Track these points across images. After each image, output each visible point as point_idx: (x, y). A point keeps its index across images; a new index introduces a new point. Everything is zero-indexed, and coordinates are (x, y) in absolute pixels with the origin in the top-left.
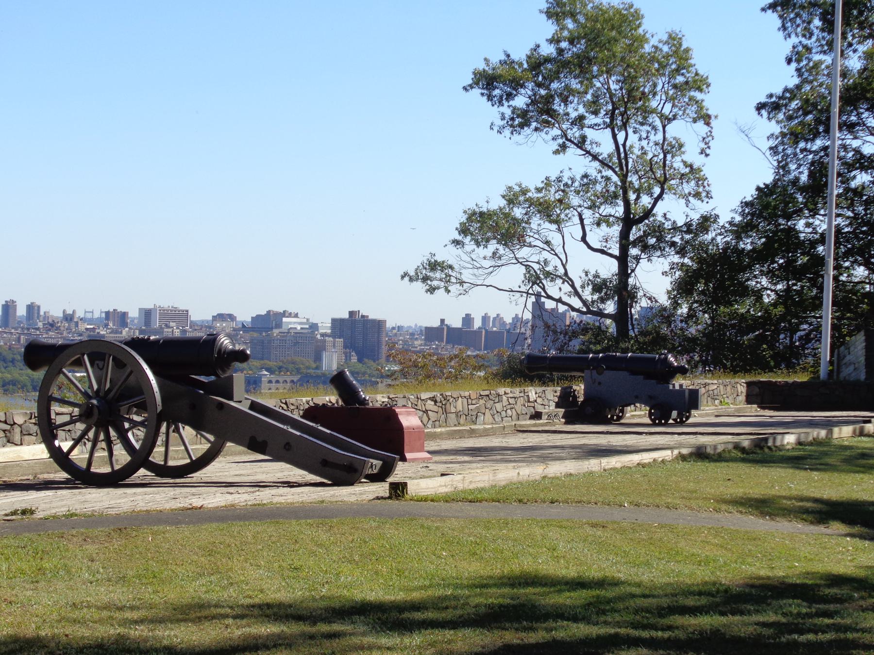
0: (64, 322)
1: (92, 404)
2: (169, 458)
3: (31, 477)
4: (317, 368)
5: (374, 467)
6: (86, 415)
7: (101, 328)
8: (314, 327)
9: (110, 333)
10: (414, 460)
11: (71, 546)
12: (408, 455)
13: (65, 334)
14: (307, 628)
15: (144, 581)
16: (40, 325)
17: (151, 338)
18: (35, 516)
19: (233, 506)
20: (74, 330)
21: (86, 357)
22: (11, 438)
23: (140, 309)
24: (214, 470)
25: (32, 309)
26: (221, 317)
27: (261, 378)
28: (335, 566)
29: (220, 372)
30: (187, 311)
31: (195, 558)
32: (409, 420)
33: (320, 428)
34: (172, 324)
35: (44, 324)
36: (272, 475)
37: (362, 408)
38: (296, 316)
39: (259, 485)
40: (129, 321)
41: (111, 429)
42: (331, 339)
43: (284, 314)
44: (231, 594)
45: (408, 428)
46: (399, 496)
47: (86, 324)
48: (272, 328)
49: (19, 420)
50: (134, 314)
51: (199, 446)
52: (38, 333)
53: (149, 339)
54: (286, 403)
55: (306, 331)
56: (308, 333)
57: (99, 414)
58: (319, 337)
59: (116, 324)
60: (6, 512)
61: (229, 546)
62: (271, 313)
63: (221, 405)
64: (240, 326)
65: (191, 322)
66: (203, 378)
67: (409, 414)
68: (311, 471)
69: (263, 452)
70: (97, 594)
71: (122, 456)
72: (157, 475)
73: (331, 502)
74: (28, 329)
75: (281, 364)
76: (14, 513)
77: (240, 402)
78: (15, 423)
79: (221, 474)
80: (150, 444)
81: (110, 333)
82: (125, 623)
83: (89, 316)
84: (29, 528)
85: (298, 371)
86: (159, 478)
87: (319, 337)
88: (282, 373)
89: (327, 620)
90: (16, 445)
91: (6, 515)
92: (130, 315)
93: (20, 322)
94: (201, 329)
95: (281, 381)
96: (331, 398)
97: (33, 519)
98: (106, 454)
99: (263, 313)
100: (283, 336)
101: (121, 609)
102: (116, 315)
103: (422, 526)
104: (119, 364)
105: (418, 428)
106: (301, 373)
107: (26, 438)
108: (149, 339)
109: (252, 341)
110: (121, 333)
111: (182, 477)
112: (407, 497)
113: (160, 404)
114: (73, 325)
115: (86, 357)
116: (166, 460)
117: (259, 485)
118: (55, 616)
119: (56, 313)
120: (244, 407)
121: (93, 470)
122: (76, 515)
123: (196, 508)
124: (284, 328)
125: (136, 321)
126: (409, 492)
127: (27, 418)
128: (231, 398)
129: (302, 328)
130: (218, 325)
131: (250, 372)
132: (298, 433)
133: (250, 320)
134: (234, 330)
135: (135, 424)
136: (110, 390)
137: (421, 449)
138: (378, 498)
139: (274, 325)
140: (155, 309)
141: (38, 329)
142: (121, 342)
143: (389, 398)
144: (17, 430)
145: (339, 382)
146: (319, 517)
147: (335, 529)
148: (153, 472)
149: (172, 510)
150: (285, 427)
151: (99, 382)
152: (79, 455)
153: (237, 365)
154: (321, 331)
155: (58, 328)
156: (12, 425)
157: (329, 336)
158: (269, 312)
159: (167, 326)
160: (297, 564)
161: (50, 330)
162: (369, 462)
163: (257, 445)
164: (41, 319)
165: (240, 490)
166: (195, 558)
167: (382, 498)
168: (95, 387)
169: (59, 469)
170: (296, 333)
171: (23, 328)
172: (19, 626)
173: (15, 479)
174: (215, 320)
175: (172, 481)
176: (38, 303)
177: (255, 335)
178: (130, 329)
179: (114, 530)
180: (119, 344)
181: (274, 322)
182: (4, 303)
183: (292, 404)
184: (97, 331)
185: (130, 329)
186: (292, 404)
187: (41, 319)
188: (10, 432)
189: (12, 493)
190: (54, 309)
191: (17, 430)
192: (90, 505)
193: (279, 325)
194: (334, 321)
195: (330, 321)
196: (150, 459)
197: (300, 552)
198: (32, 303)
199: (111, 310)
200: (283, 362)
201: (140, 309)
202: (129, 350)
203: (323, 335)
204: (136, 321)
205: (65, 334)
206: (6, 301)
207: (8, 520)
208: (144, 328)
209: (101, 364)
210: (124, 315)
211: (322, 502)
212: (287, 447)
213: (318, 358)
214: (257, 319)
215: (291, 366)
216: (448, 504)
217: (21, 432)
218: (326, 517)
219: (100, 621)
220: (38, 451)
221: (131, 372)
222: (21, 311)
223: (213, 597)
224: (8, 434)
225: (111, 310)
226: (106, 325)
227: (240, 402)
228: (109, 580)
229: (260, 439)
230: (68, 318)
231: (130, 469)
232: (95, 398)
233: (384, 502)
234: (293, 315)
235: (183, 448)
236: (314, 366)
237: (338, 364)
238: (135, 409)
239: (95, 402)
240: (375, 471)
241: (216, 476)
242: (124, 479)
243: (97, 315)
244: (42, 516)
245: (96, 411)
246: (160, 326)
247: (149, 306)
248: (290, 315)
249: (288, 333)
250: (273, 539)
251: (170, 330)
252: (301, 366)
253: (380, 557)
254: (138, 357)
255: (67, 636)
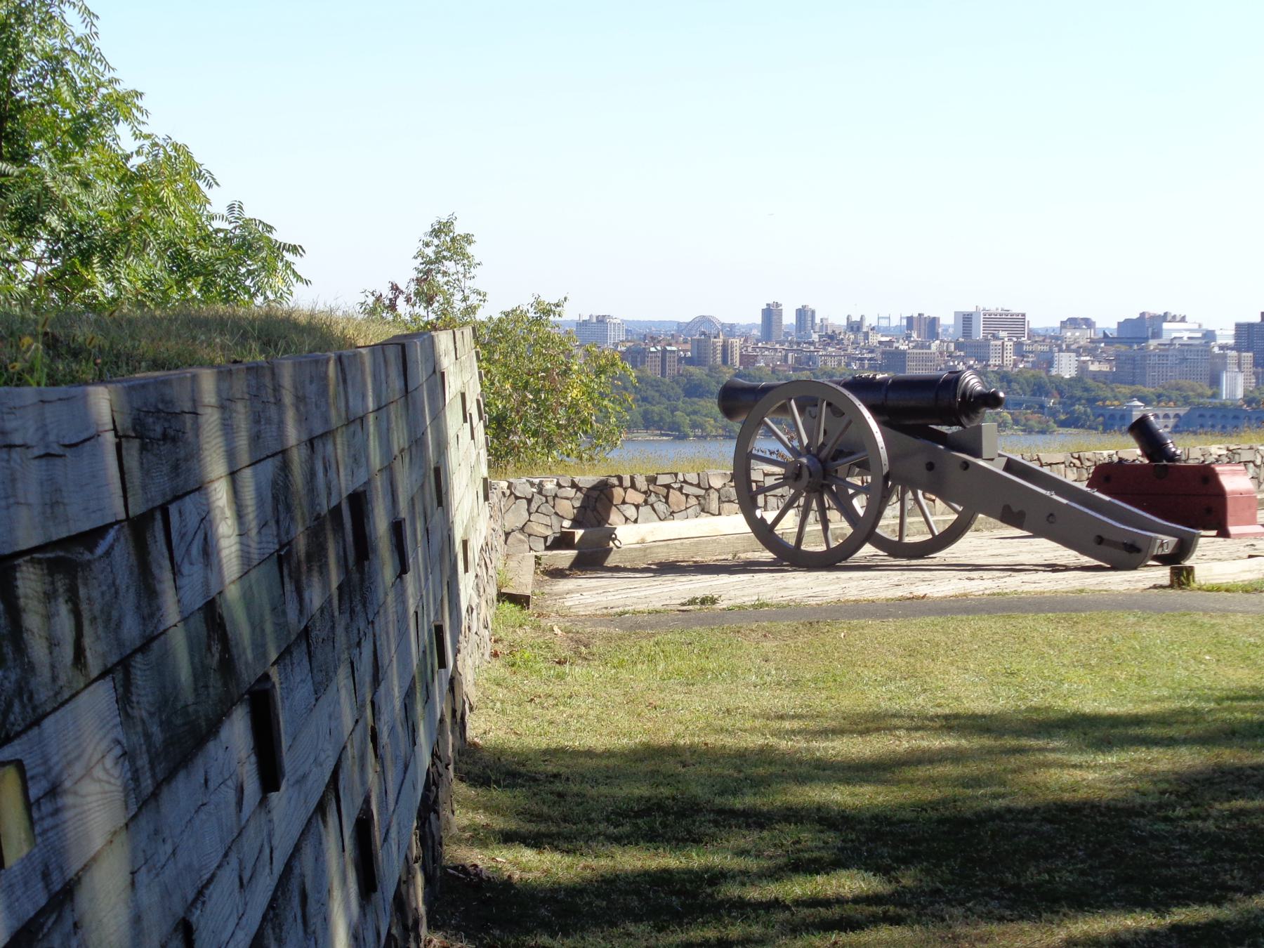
0: (848, 333)
1: (802, 464)
2: (906, 532)
3: (730, 557)
4: (1214, 396)
5: (1165, 545)
6: (793, 476)
7: (901, 341)
8: (1209, 336)
9: (914, 348)
10: (1240, 536)
11: (746, 643)
12: (1232, 529)
13: (850, 350)
14: (987, 741)
15: (821, 685)
16: (815, 337)
17: (878, 377)
18: (717, 606)
19: (965, 595)
20: (862, 344)
21: (793, 402)
22: (706, 507)
23: (956, 313)
24: (962, 550)
25: (803, 315)
26: (1073, 323)
27: (1131, 411)
28: (1063, 671)
29: (964, 420)
30: (1024, 315)
31: (891, 658)
32: (1234, 481)
33: (1097, 494)
34: (1002, 334)
35: (820, 337)
36: (1039, 555)
37: (1171, 467)
38: (1183, 320)
39: (1014, 569)
40: (940, 330)
41: (826, 497)
42: (1234, 353)
43: (1164, 318)
44: (920, 703)
45: (1233, 492)
46: (1184, 584)
47: (879, 335)
48: (1146, 339)
49: (717, 483)
50: (947, 319)
51: (942, 515)
52: (812, 348)
53: (874, 378)
54: (1079, 458)
55: (1197, 342)
56: (1201, 345)
57: (811, 475)
58: (1216, 350)
59: (922, 335)
60: (683, 601)
61: (938, 645)
62: (1147, 316)
63: (966, 465)
64: (1101, 335)
65: (1030, 330)
66: (944, 429)
67: (1234, 473)
68: (1083, 551)
69: (1019, 526)
70: (757, 700)
71: (840, 526)
72: (890, 555)
73: (1093, 592)
74: (798, 344)
75: (1161, 390)
76: (693, 602)
77: (992, 460)
78: (710, 487)
79: (974, 553)
80: (876, 512)
81: (914, 348)
82: (777, 733)
83: (884, 323)
84: (702, 621)
85: (1186, 401)
86: (892, 559)
87: (1216, 350)
88: (1163, 404)
89: (1018, 733)
90: (713, 515)
91: (683, 604)
92: (941, 322)
93: (788, 334)
94: (1044, 341)
95: (1172, 416)
96: (1133, 452)
97: (714, 610)
98: (820, 527)
99: (1135, 316)
100: (1164, 350)
101: (782, 717)
102: (923, 322)
103: (1194, 623)
104: (835, 410)
105: (1249, 492)
106: (1190, 404)
107: (726, 505)
108: (874, 378)
109: (1117, 357)
110: (929, 347)
111: (921, 557)
112: (1194, 585)
113: (887, 463)
114: (861, 337)
115: (793, 402)
116: (901, 536)
117: (1014, 569)
118: (701, 724)
119: (837, 320)
120: (997, 468)
121: (907, 540)
122: (767, 605)
123: (918, 598)
124: (1165, 338)
125: (951, 330)
126: (1196, 579)
127: (726, 481)
128: (978, 454)
129: (1189, 338)
130: (1069, 334)
131: (1116, 403)
132: (1064, 501)
133: (1115, 326)
134: (1092, 341)
135: (859, 490)
136: (823, 444)
137: (1252, 521)
138: (1155, 587)
139: (1150, 334)
140: (977, 312)
141: (812, 343)
142: (838, 383)
143: (1228, 450)
144: (714, 496)
145: (1142, 431)
146: (1062, 610)
147: (1080, 626)
148: (884, 551)
149: (887, 600)
150: (1048, 493)
151: (809, 437)
152: (789, 524)
153: (988, 412)
154: (1220, 341)
155: (840, 342)
156: (707, 490)
157: (1232, 349)
158: (1143, 314)
159: (995, 337)
160: (1015, 667)
161: (828, 344)
162: (1156, 539)
163: (1012, 517)
164: (817, 329)
165: (985, 574)
166: (891, 658)
167: (1162, 587)
168: (806, 441)
169: (761, 546)
170: (1182, 345)
171: (791, 343)
172: (655, 734)
173: (709, 559)
174: (1065, 328)
175: (905, 562)
176: (811, 306)
177: (1123, 348)
178: (942, 341)
179: (803, 624)
180: (834, 386)
181: (1150, 330)
182: (765, 307)
183: (1088, 460)
184: (896, 345)
185: (942, 341)
186: (1088, 460)
187: (817, 329)
188: (705, 499)
189: (700, 577)
190: (834, 314)
191: (714, 496)
192: (790, 593)
193: (1157, 334)
194: (1239, 327)
195: (1233, 327)
196: (878, 530)
197: (1024, 654)
198: (804, 307)
199: (916, 315)
200: (1163, 387)
201: (956, 313)
202: (846, 392)
203: (1222, 347)
204: (951, 330)
205: (850, 350)
206: (768, 305)
207: (683, 611)
208: (961, 340)
209: (813, 410)
210: (933, 322)
211: (1082, 591)
212: (1050, 519)
213: (1215, 381)
214: (1125, 325)
215: (1174, 394)
216: (1246, 595)
217: (719, 498)
218: (1076, 610)
219: (753, 730)
220: (734, 524)
221: (850, 422)
222: (789, 319)
223: (896, 706)
224: (702, 501)
225: (916, 315)
226: (908, 337)
227: (992, 460)
228: (779, 684)
229: (1015, 509)
230: (855, 327)
231: (851, 546)
232: (804, 456)
233: (1161, 591)
234: (1178, 319)
235: (923, 519)
236: (1209, 392)
237: (1245, 390)
238: (857, 470)
239: (804, 460)
240: (1167, 551)
241: (966, 557)
242: (845, 559)
243: (895, 322)
244: (725, 607)
245: (805, 473)
246: (986, 340)
247: (969, 308)
248: (1174, 319)
249: (1171, 344)
250: (996, 637)
251: (999, 342)
252: (1191, 393)
253: (1124, 661)
254: (858, 403)
255: (706, 744)
